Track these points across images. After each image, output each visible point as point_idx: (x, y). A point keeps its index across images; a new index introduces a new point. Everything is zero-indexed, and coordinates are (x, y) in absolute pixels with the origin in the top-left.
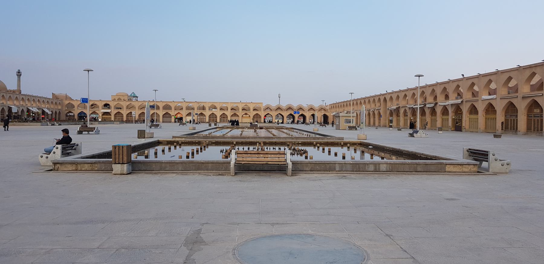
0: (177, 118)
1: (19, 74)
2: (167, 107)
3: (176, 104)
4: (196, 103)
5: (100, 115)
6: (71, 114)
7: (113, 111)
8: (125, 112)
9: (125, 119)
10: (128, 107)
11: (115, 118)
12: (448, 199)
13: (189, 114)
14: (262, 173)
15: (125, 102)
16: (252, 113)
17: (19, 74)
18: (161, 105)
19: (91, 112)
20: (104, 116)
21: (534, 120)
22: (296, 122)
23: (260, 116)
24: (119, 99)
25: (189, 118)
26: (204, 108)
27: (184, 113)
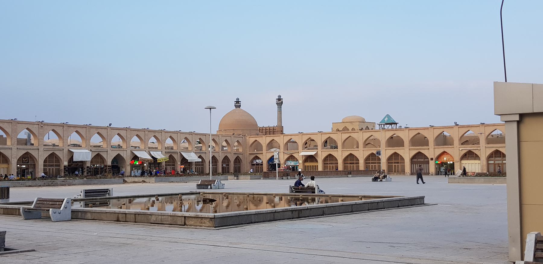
0: (442, 164)
1: (280, 102)
2: (419, 140)
3: (488, 130)
4: (482, 129)
5: (301, 162)
6: (258, 161)
7: (319, 153)
8: (340, 155)
9: (340, 168)
10: (367, 144)
11: (325, 167)
12: (34, 251)
13: (470, 155)
14: (37, 220)
15: (339, 133)
16: (484, 150)
17: (280, 102)
18: (431, 137)
19: (286, 157)
20: (307, 164)
21: (53, 169)
22: (232, 170)
23: (403, 159)
24: (345, 129)
25: (473, 166)
26: (424, 142)
27: (455, 152)
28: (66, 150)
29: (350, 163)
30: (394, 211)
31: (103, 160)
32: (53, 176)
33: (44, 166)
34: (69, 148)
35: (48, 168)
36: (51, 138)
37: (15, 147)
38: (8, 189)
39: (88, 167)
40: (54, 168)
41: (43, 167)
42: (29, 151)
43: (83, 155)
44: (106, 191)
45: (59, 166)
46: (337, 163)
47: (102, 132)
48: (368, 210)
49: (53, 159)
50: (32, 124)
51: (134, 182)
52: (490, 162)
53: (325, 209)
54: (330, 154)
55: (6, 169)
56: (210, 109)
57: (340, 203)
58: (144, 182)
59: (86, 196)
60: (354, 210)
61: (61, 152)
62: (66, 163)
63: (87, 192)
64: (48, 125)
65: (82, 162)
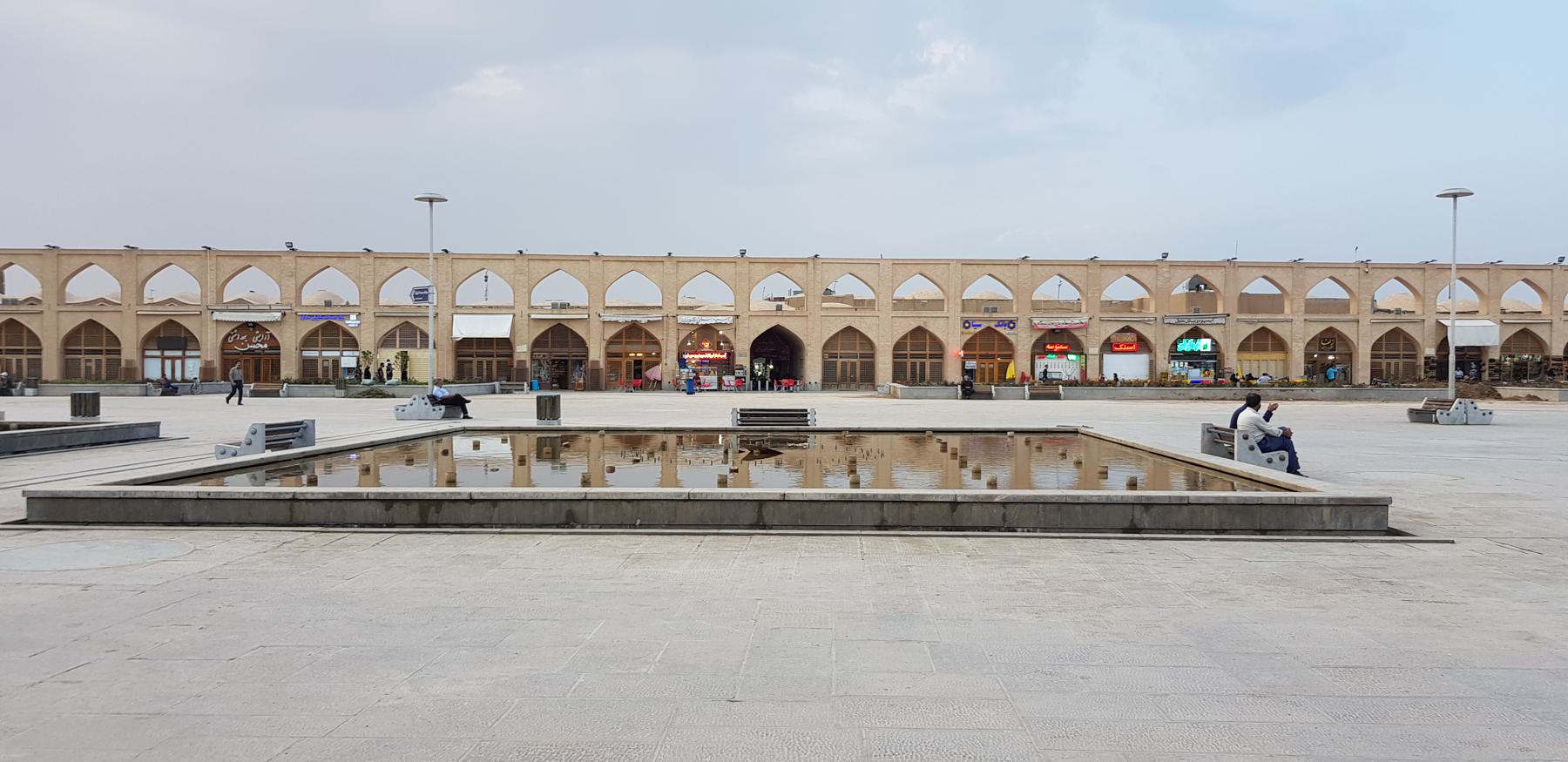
21: (19, 361)
28: (1430, 322)
29: (913, 356)
30: (938, 544)
31: (1539, 344)
32: (1396, 377)
33: (1373, 356)
34: (1439, 317)
35: (1384, 362)
36: (1391, 295)
37: (1299, 318)
38: (96, 396)
39: (1492, 360)
40: (1401, 361)
41: (1368, 360)
42: (1334, 325)
43: (1483, 332)
44: (801, 415)
45: (1414, 356)
46: (39, 352)
47: (1541, 279)
48: (879, 527)
49: (1395, 342)
50: (1346, 267)
51: (1516, 399)
52: (148, 353)
53: (1011, 510)
54: (12, 320)
55: (1280, 364)
56: (431, 201)
57: (1180, 491)
58: (1536, 398)
59: (743, 423)
60: (767, 520)
61: (1418, 327)
62: (1431, 351)
63: (746, 415)
64: (1382, 267)
65: (1478, 348)
